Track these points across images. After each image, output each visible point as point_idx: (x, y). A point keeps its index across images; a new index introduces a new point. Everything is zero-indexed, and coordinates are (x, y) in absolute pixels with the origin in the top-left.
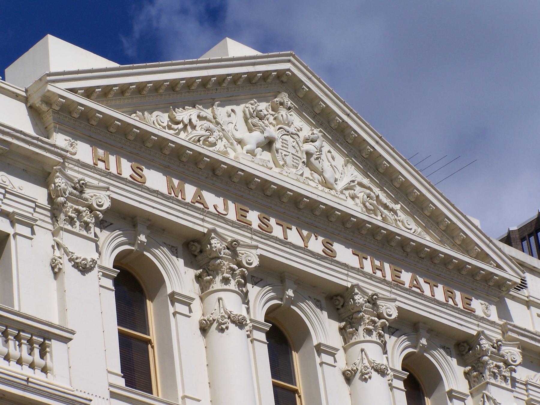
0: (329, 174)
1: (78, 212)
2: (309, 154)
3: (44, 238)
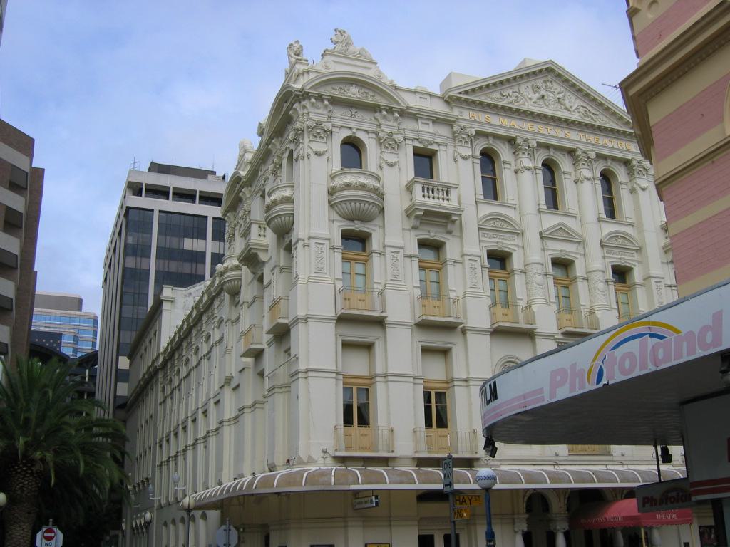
0: (568, 105)
1: (463, 138)
2: (559, 99)
3: (451, 149)
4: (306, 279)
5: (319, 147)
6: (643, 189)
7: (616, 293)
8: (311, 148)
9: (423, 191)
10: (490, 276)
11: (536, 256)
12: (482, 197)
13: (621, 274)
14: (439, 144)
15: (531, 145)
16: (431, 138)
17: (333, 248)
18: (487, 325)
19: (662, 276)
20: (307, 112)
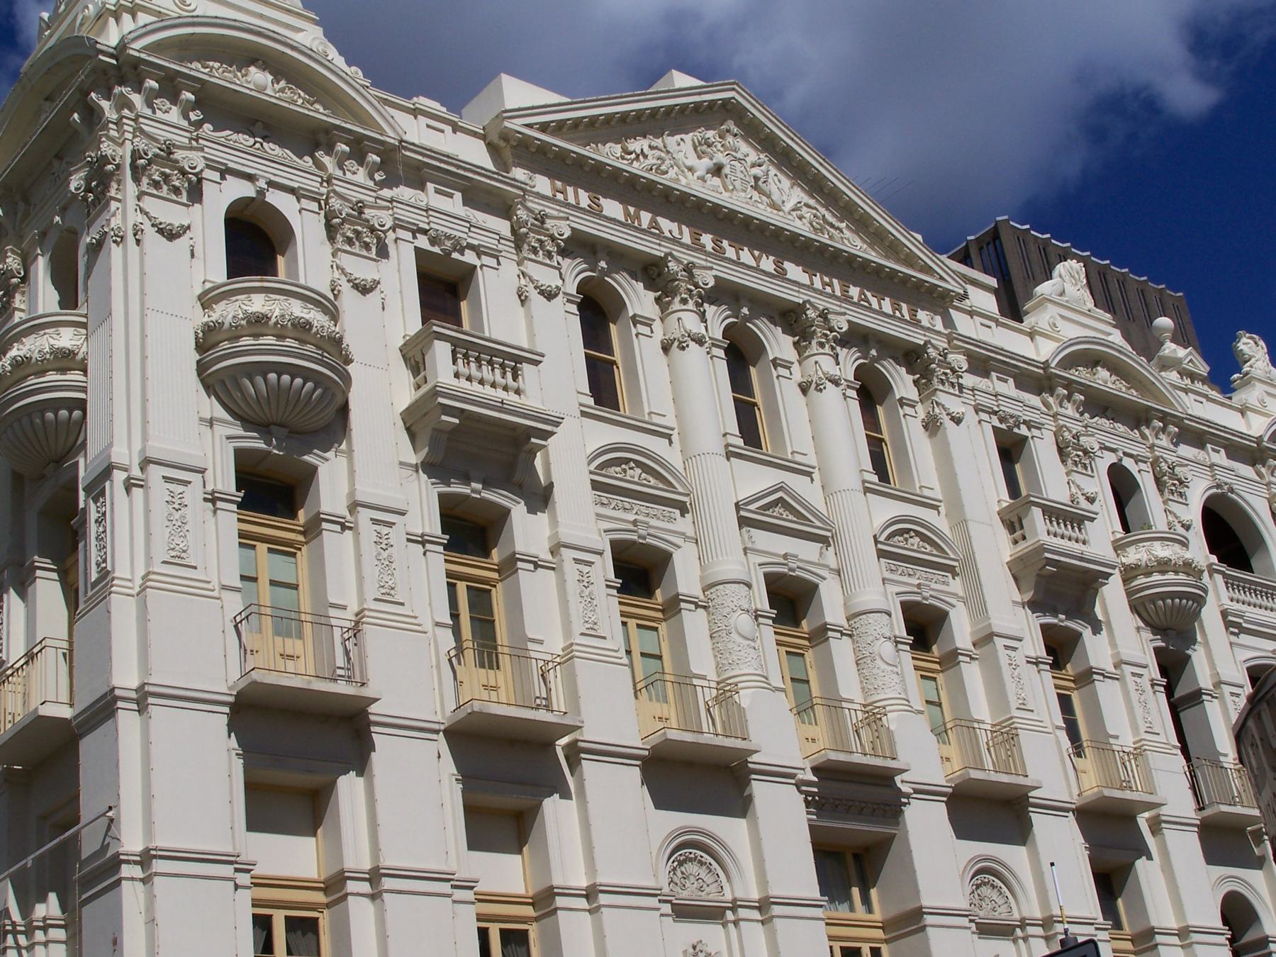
0: (776, 197)
4: (139, 582)
5: (172, 214)
6: (957, 420)
7: (624, 624)
8: (146, 214)
9: (454, 361)
10: (242, 535)
11: (731, 563)
12: (740, 442)
13: (923, 627)
14: (1029, 425)
15: (834, 324)
16: (459, 231)
17: (213, 498)
18: (222, 676)
19: (1144, 662)
20: (132, 116)
